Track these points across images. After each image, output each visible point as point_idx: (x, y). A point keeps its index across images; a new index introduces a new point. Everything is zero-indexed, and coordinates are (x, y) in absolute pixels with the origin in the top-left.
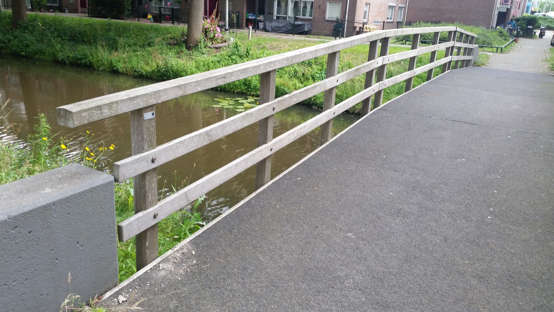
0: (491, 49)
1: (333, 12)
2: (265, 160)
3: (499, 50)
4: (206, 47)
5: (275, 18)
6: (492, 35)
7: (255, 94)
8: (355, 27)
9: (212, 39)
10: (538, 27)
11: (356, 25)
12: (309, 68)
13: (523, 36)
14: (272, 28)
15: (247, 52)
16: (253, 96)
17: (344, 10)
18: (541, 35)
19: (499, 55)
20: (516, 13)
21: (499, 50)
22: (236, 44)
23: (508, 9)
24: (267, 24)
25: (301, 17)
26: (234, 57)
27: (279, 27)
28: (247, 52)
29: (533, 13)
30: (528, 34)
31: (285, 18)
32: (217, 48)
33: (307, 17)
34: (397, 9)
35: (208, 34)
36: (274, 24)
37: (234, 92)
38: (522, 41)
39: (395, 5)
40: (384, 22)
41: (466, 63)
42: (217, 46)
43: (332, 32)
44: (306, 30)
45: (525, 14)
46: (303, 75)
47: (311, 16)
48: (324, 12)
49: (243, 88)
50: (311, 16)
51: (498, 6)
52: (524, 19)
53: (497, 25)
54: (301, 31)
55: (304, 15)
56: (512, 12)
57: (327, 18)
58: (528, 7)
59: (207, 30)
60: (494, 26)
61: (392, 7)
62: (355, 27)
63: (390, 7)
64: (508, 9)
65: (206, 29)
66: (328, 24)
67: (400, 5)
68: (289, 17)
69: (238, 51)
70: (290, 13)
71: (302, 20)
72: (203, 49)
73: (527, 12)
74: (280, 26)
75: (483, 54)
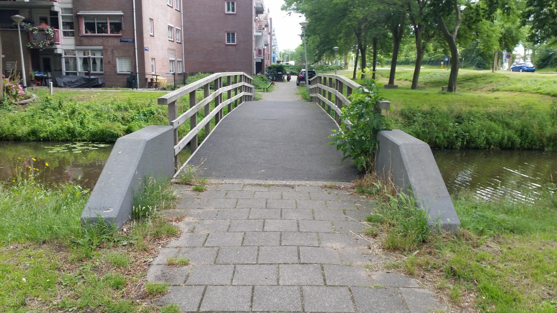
0: (259, 90)
1: (123, 67)
2: (209, 122)
3: (265, 91)
4: (11, 104)
5: (64, 74)
6: (256, 79)
7: (81, 139)
8: (147, 79)
9: (15, 97)
10: (285, 73)
11: (147, 76)
12: (127, 113)
13: (276, 81)
14: (64, 84)
15: (60, 104)
16: (79, 141)
17: (133, 64)
18: (289, 79)
19: (266, 94)
20: (268, 63)
21: (265, 91)
22: (47, 98)
23: (262, 60)
24: (58, 79)
25: (92, 72)
26: (47, 110)
27: (72, 83)
28: (60, 104)
29: (278, 62)
30: (279, 79)
31: (75, 74)
32: (22, 104)
33: (98, 71)
34: (176, 62)
35: (10, 92)
36: (66, 80)
37: (58, 141)
38: (277, 84)
39: (174, 59)
40: (174, 74)
41: (247, 98)
42: (22, 102)
43: (126, 84)
44: (100, 83)
45: (273, 64)
46: (123, 118)
47: (102, 70)
48: (115, 66)
49: (67, 135)
50: (102, 70)
51: (255, 57)
52: (274, 67)
53: (257, 73)
54: (97, 84)
55: (94, 70)
56: (266, 61)
57: (118, 71)
58: (274, 58)
59: (9, 88)
60: (255, 73)
61: (172, 61)
62: (147, 79)
63: (170, 61)
64: (262, 60)
65: (7, 87)
66: (120, 77)
67: (178, 60)
68: (79, 73)
69: (50, 104)
70: (80, 69)
71: (93, 74)
72: (8, 106)
73: (274, 62)
74: (73, 81)
75: (257, 93)
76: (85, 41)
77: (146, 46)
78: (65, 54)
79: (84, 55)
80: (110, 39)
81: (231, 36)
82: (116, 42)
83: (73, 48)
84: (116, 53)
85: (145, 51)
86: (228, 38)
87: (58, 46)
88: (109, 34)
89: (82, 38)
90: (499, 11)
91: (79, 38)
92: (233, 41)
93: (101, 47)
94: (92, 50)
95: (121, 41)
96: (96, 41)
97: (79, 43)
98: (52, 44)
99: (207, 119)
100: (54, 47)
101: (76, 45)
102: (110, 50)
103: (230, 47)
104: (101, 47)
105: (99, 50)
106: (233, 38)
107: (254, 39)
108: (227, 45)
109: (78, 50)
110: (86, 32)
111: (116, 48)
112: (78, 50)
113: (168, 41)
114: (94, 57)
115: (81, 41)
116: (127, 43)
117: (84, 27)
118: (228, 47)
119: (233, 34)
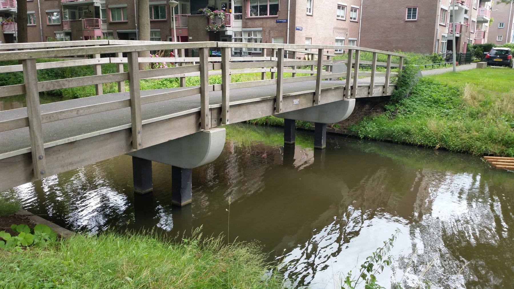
39: (344, 38)
68: (244, 52)
76: (250, 23)
77: (297, 25)
78: (235, 36)
79: (249, 36)
80: (268, 20)
81: (412, 11)
82: (273, 23)
83: (240, 30)
84: (272, 34)
85: (297, 31)
86: (409, 13)
87: (228, 28)
88: (268, 15)
89: (247, 21)
90: (476, 280)
91: (245, 20)
92: (414, 16)
93: (261, 29)
94: (255, 32)
95: (277, 22)
96: (258, 23)
97: (245, 26)
98: (223, 27)
99: (65, 141)
100: (225, 29)
101: (243, 27)
102: (268, 31)
103: (410, 24)
104: (159, 30)
105: (260, 31)
106: (415, 13)
107: (439, 12)
108: (407, 21)
109: (245, 32)
110: (251, 15)
111: (272, 29)
112: (245, 32)
113: (336, 20)
114: (255, 37)
115: (246, 23)
116: (281, 24)
117: (250, 10)
118: (408, 23)
119: (415, 10)
